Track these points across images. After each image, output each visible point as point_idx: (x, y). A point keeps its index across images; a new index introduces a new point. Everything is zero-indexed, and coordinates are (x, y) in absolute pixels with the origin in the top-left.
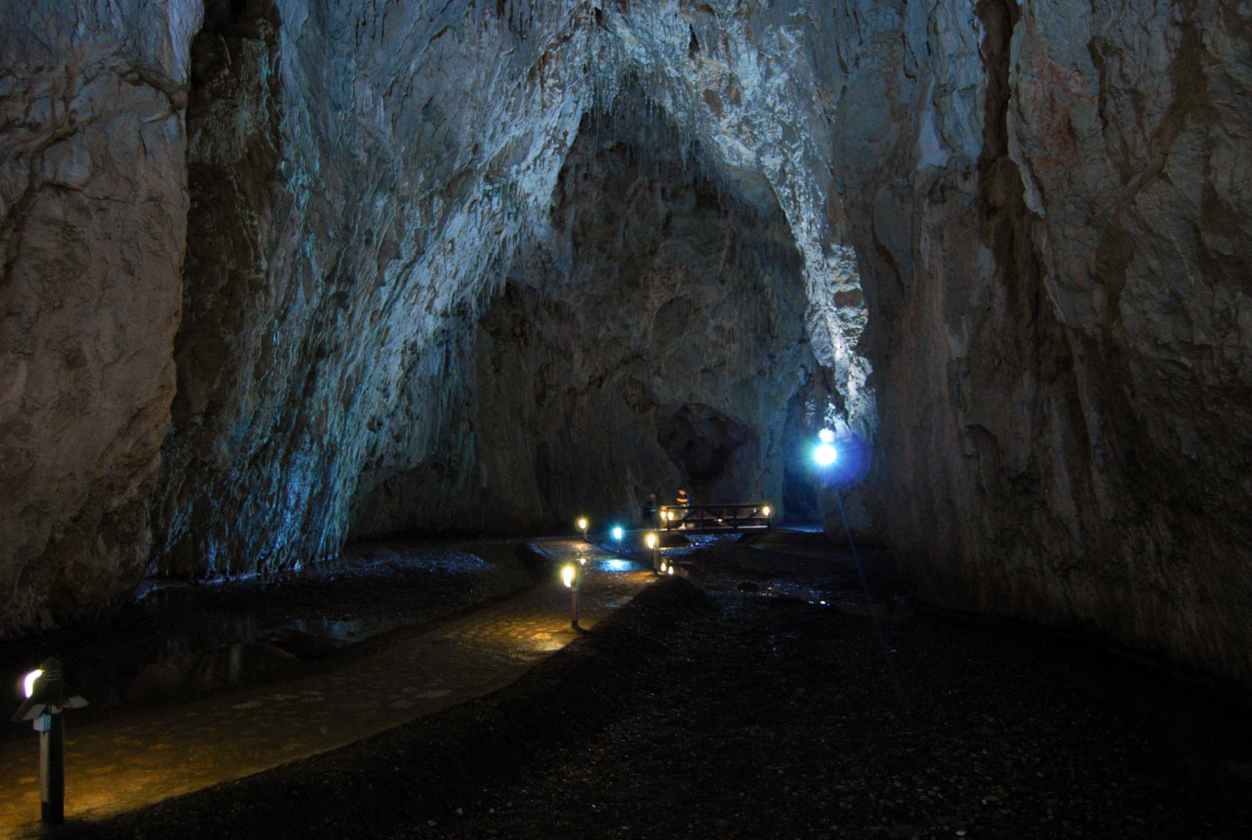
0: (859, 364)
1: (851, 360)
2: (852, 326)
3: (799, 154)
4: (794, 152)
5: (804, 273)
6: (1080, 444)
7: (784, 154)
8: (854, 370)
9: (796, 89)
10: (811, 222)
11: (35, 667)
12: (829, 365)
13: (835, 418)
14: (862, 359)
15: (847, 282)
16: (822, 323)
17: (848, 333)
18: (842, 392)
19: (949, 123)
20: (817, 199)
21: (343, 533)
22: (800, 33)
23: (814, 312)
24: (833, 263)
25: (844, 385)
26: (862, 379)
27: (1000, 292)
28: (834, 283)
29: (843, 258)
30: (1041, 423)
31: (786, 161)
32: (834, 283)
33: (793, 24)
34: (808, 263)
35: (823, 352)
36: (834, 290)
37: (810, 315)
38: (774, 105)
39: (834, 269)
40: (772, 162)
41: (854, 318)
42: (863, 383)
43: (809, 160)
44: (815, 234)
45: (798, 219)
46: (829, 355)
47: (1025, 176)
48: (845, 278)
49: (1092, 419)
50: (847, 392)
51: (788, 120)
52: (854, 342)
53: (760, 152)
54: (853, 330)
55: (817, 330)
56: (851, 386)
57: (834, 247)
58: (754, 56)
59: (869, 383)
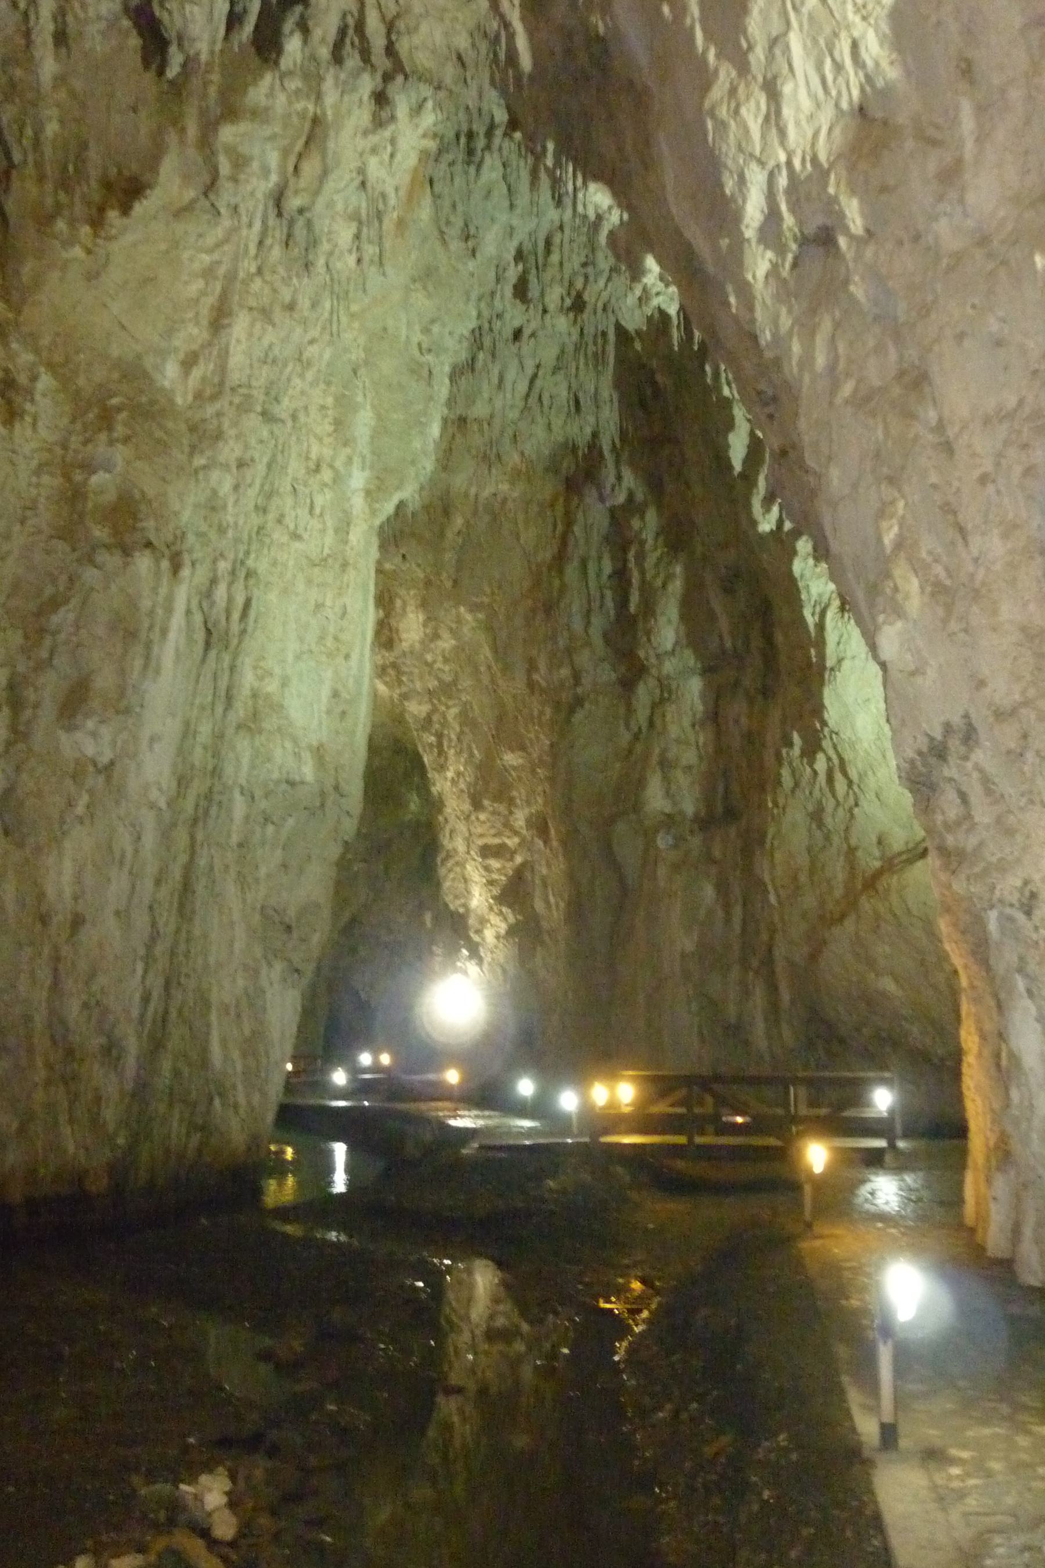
0: (501, 913)
1: (491, 909)
2: (495, 876)
3: (454, 711)
4: (448, 707)
5: (441, 818)
6: (774, 1008)
7: (433, 704)
8: (495, 919)
9: (464, 656)
10: (459, 774)
11: (449, 1126)
12: (461, 910)
13: (468, 964)
14: (504, 909)
15: (495, 835)
16: (458, 869)
17: (491, 883)
18: (476, 938)
19: (674, 787)
20: (471, 755)
21: (998, 1037)
22: (481, 616)
23: (448, 856)
24: (482, 817)
25: (479, 932)
26: (503, 927)
27: (720, 913)
28: (481, 836)
29: (494, 813)
30: (746, 993)
31: (435, 710)
32: (481, 836)
33: (474, 608)
34: (448, 810)
35: (456, 897)
36: (480, 842)
37: (444, 861)
38: (434, 662)
39: (484, 822)
40: (417, 709)
41: (498, 870)
42: (503, 932)
43: (466, 719)
44: (462, 786)
45: (442, 768)
46: (463, 901)
47: (770, 888)
48: (493, 831)
49: (785, 996)
50: (483, 939)
51: (448, 678)
52: (496, 891)
53: (405, 697)
54: (496, 881)
55: (451, 875)
56: (489, 934)
57: (486, 802)
58: (421, 617)
59: (512, 931)
